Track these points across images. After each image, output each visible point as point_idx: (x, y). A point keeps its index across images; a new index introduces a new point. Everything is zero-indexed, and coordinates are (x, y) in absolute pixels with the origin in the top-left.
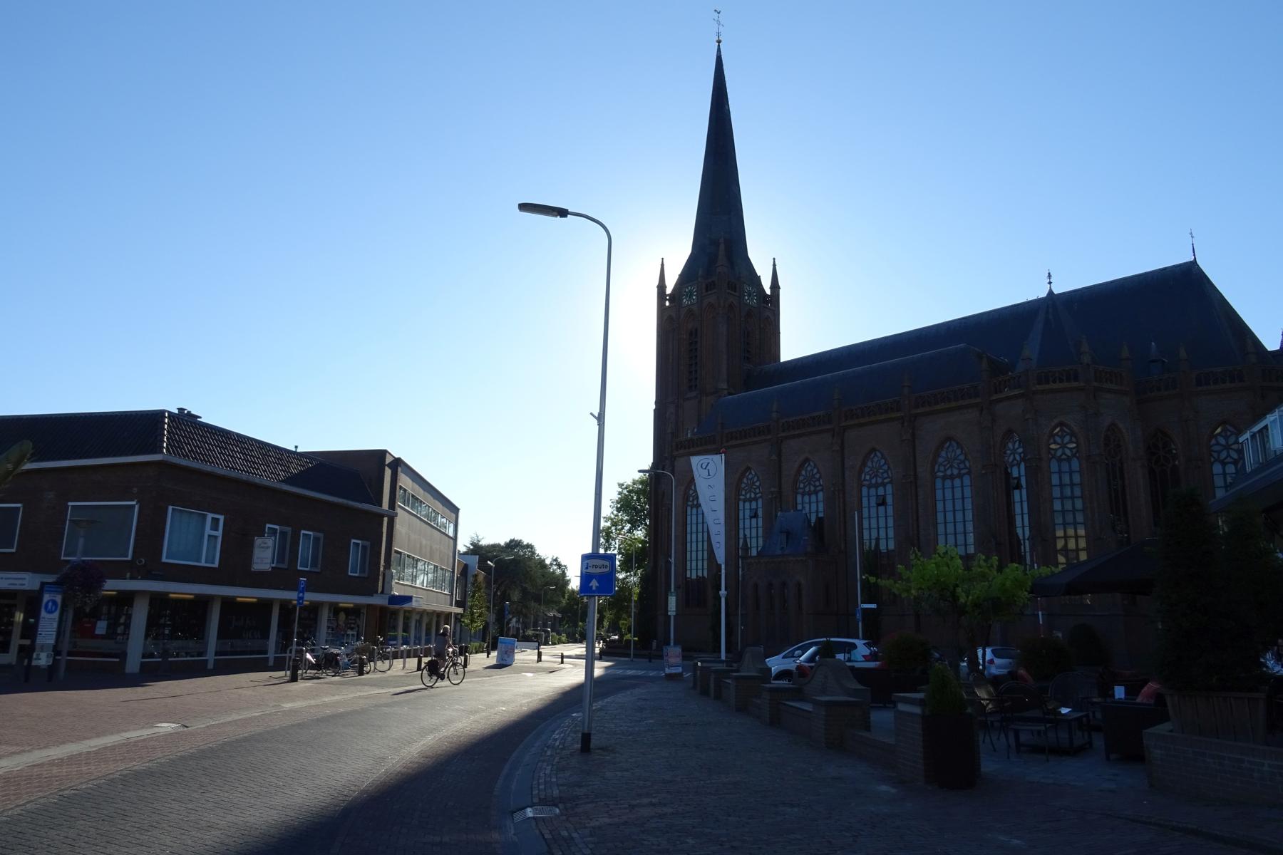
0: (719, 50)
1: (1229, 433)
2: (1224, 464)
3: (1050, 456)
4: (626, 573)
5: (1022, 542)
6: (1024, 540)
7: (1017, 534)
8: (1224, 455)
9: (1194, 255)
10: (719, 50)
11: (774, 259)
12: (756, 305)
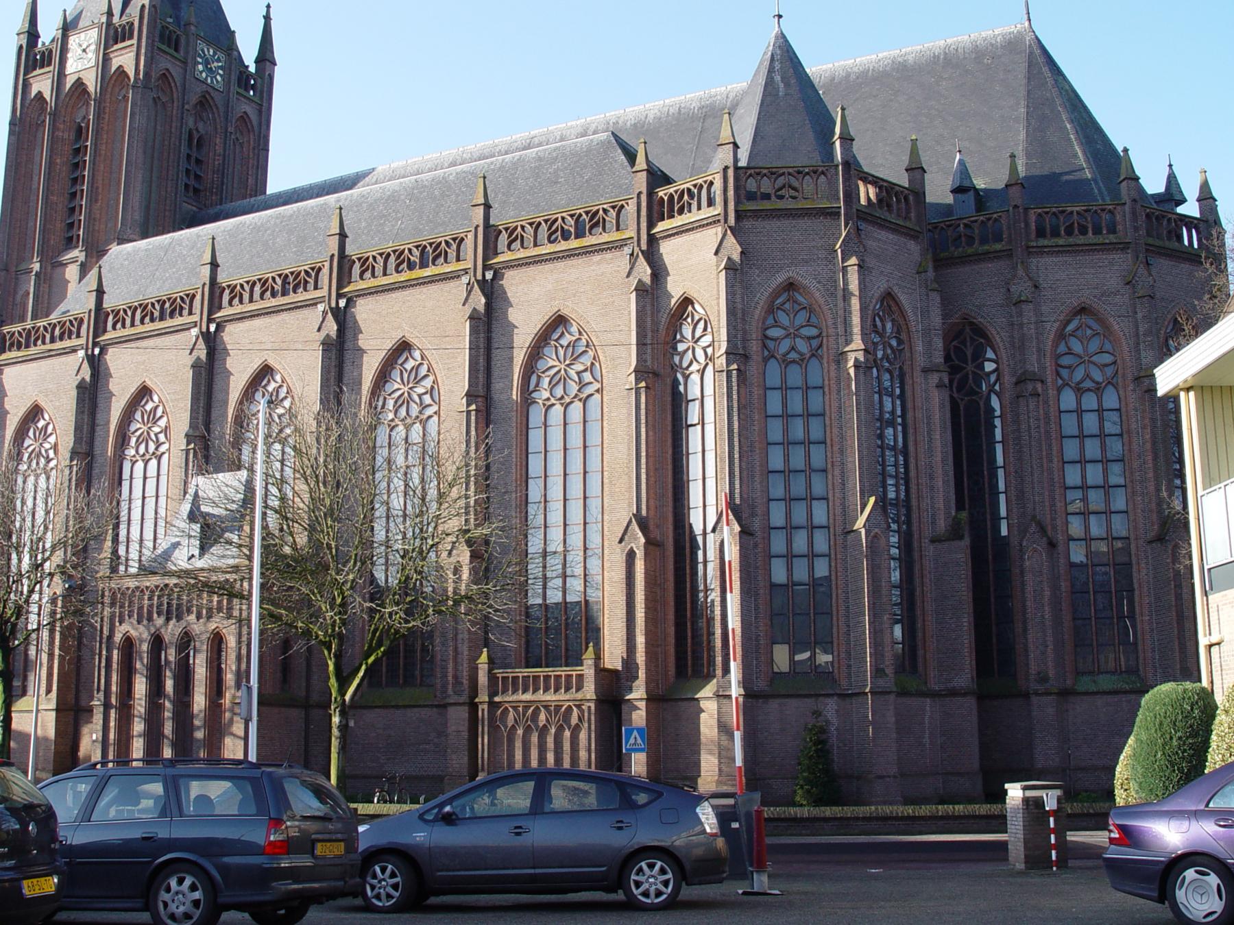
1: (1089, 332)
2: (1079, 391)
3: (766, 353)
4: (356, 810)
5: (700, 539)
6: (705, 534)
7: (691, 526)
8: (1079, 374)
9: (1029, 20)
11: (268, 6)
12: (220, 87)
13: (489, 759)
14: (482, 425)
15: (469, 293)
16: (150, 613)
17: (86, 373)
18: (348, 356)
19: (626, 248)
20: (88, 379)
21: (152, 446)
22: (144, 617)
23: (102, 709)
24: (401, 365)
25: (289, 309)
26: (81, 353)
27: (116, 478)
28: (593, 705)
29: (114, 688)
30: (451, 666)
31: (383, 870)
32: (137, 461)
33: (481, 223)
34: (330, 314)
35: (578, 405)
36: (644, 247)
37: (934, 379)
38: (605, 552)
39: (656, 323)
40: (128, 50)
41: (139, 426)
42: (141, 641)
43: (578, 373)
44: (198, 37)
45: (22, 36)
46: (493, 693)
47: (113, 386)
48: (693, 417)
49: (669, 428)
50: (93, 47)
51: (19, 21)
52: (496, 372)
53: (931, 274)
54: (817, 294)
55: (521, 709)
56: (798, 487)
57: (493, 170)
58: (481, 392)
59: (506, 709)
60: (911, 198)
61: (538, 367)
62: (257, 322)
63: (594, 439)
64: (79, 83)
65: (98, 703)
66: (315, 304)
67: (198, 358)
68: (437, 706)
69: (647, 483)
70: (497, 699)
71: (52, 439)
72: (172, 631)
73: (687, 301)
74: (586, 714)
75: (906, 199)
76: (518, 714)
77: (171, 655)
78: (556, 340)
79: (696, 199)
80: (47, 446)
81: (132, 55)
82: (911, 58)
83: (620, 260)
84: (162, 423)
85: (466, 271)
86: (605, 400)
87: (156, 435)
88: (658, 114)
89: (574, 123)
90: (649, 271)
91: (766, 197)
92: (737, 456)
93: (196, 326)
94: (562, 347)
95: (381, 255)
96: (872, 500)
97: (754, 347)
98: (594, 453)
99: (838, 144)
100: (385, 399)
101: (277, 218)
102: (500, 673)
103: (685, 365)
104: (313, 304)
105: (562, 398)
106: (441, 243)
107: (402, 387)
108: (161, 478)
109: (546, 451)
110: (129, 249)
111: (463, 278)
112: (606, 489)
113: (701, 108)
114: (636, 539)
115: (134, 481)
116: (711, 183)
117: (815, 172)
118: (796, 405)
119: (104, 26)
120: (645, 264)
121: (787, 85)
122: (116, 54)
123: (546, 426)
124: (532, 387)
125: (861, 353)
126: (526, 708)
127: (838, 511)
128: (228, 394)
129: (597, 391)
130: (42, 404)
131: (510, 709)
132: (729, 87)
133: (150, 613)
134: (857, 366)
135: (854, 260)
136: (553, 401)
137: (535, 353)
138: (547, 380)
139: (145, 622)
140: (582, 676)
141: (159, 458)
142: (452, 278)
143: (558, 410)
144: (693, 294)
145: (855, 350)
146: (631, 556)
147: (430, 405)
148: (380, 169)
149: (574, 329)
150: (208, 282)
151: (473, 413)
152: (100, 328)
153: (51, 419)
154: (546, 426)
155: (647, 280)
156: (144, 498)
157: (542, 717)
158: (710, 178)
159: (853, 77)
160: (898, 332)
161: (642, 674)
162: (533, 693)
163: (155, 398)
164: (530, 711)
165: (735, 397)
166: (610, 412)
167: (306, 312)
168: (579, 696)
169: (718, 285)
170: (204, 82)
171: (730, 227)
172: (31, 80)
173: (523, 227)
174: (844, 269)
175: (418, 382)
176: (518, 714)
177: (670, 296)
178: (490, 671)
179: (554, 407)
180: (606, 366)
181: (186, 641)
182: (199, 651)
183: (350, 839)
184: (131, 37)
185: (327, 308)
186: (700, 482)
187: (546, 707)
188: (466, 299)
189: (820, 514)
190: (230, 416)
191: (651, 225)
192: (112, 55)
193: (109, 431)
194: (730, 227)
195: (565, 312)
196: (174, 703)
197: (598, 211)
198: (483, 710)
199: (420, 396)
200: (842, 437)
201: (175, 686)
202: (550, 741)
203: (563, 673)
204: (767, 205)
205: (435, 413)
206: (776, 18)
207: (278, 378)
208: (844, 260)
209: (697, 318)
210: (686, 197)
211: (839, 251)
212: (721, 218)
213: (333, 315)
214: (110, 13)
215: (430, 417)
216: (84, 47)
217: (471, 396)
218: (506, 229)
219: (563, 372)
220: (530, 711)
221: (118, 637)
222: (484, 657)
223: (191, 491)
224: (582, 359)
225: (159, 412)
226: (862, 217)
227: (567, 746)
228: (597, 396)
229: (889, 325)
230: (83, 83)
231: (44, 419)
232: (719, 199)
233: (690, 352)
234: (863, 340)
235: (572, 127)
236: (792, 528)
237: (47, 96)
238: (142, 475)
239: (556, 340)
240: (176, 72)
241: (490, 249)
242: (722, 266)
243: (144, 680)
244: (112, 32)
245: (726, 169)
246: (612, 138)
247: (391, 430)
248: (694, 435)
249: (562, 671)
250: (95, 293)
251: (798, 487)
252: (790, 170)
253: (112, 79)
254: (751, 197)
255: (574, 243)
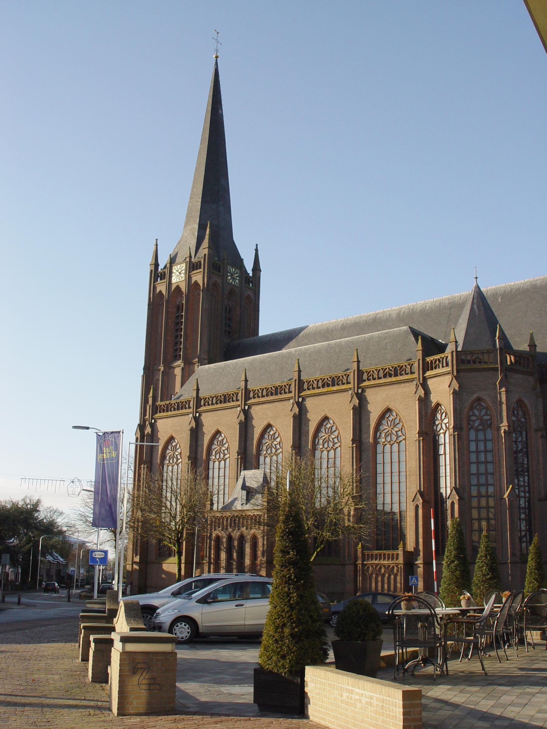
0: (216, 64)
10: (216, 64)
11: (257, 245)
12: (238, 285)
13: (362, 586)
14: (358, 461)
15: (352, 398)
16: (227, 526)
17: (193, 424)
18: (303, 422)
19: (414, 382)
20: (194, 426)
21: (222, 456)
22: (225, 529)
23: (207, 564)
24: (325, 426)
25: (278, 401)
26: (191, 415)
27: (207, 468)
28: (402, 566)
29: (212, 556)
30: (347, 549)
31: (335, 617)
32: (215, 461)
33: (356, 369)
34: (295, 404)
35: (396, 445)
36: (421, 382)
37: (540, 434)
38: (408, 504)
39: (426, 413)
40: (199, 274)
41: (216, 447)
42: (223, 538)
43: (396, 432)
44: (228, 264)
45: (152, 266)
46: (363, 560)
47: (205, 429)
48: (441, 451)
49: (432, 455)
50: (183, 272)
51: (150, 259)
52: (363, 430)
53: (539, 389)
54: (489, 403)
55: (374, 567)
56: (483, 480)
57: (361, 341)
58: (358, 438)
59: (369, 566)
60: (530, 359)
61: (380, 428)
62: (265, 406)
63: (403, 459)
64: (178, 288)
65: (206, 562)
66: (289, 400)
67: (241, 420)
68: (341, 565)
69: (423, 478)
70: (365, 563)
71: (179, 451)
72: (236, 534)
73: (438, 405)
74: (400, 569)
75: (528, 359)
76: (373, 568)
77: (236, 543)
78: (387, 418)
79: (441, 362)
80: (177, 453)
81: (201, 276)
82: (538, 282)
83: (412, 387)
84: (226, 446)
85: (350, 389)
86: (407, 443)
87: (224, 451)
88: (431, 305)
89: (395, 308)
90: (423, 392)
91: (469, 362)
92: (457, 468)
93: (239, 406)
94: (390, 421)
95: (316, 380)
96: (511, 486)
97: (464, 424)
98: (403, 464)
99: (497, 341)
100: (319, 440)
101: (270, 358)
102: (366, 552)
103: (438, 430)
104: (289, 399)
105: (390, 442)
106: (340, 376)
107: (325, 435)
108: (226, 468)
109: (384, 463)
110: (207, 368)
111: (349, 391)
112: (407, 479)
113: (449, 303)
114: (419, 500)
115: (215, 470)
116: (447, 357)
117: (488, 352)
118: (482, 447)
119: (188, 263)
120: (422, 389)
121: (479, 310)
122: (194, 275)
123: (384, 453)
124: (378, 437)
125: (507, 427)
126: (376, 566)
127: (498, 489)
128: (253, 435)
129: (404, 439)
130: (174, 436)
131: (370, 567)
132: (461, 294)
133: (227, 526)
134: (505, 431)
135: (504, 389)
136: (386, 443)
137: (379, 423)
138: (384, 434)
139: (225, 530)
140: (398, 554)
141: (225, 460)
142: (345, 391)
143: (388, 447)
144: (441, 402)
145: (504, 426)
146: (417, 507)
147: (337, 443)
148: (310, 326)
149: (394, 414)
150: (244, 388)
151: (355, 448)
152: (198, 405)
153: (178, 442)
154: (384, 453)
155: (423, 396)
156: (219, 477)
157: (383, 570)
158: (447, 355)
159: (514, 291)
160: (524, 415)
161: (421, 554)
162: (379, 560)
163: (223, 435)
164: (378, 567)
165: (457, 445)
166: (409, 448)
167: (285, 402)
168: (397, 562)
169: (450, 400)
170: (231, 284)
171: (454, 376)
172: (157, 285)
173: (373, 371)
174: (500, 393)
175: (332, 433)
176: (373, 568)
177: (432, 402)
178: (362, 551)
179: (387, 446)
180: (407, 430)
181: (242, 538)
182: (247, 542)
183: (330, 609)
184: (200, 268)
185: (294, 402)
186: (444, 478)
187: (384, 566)
188: (351, 401)
189: (491, 489)
190: (255, 444)
191: (424, 373)
192: (192, 276)
193: (203, 449)
194: (454, 376)
195: (391, 407)
196: (237, 563)
197: (403, 366)
198: (359, 567)
199: (333, 439)
200: (499, 461)
201: (237, 556)
202: (386, 579)
203: (391, 553)
204: (469, 366)
205: (339, 446)
206: (475, 279)
207: (274, 429)
208: (500, 389)
209: (442, 411)
210: (437, 362)
211: (498, 385)
212: (451, 372)
213: (296, 404)
214: (190, 257)
215: (337, 448)
216: (180, 271)
217: (353, 441)
218: (366, 372)
219: (390, 431)
220: (378, 567)
221: (214, 535)
222: (360, 546)
223: (242, 476)
224: (397, 426)
225: (225, 441)
226: (507, 370)
227: (392, 581)
228: (404, 441)
229: (520, 413)
230: (179, 287)
231: (175, 442)
232: (450, 364)
233: (440, 425)
234: (507, 422)
235: (394, 310)
236: (480, 496)
237: (164, 292)
238: (218, 467)
239: (387, 418)
240: (219, 281)
241: (360, 380)
242: (451, 392)
243: (225, 553)
244: (192, 265)
245: (452, 352)
246: (409, 329)
247: (322, 452)
248: (442, 459)
249: (391, 552)
250: (196, 390)
251: (483, 480)
252: (479, 352)
253: (193, 287)
254: (463, 362)
255: (393, 379)
